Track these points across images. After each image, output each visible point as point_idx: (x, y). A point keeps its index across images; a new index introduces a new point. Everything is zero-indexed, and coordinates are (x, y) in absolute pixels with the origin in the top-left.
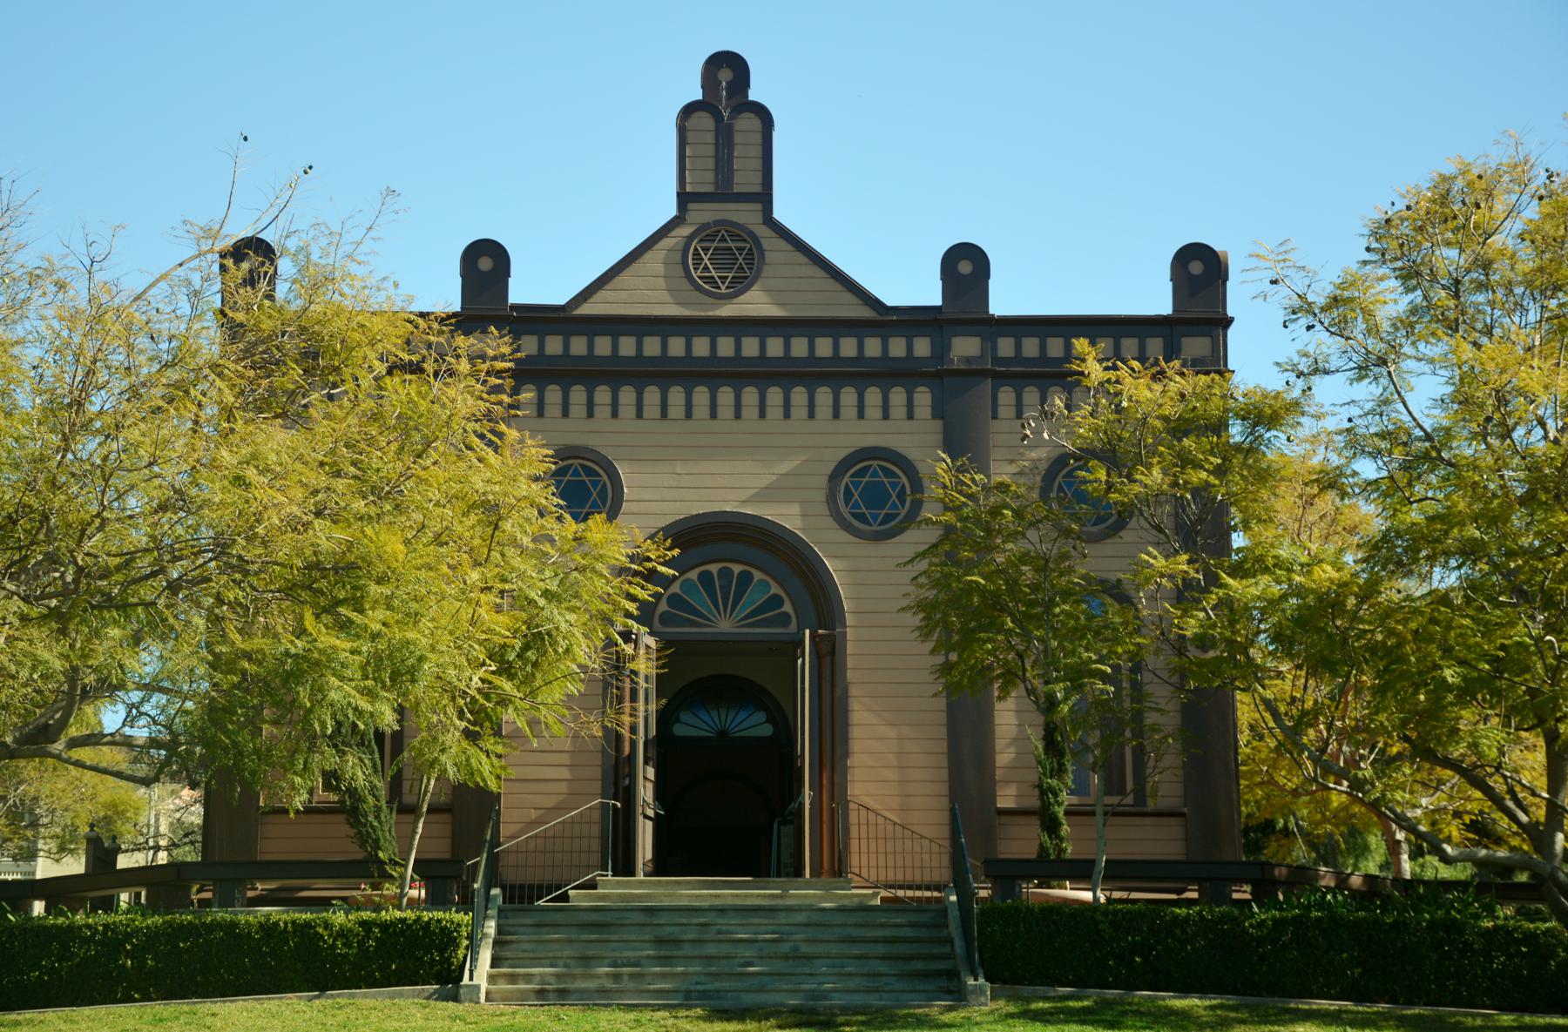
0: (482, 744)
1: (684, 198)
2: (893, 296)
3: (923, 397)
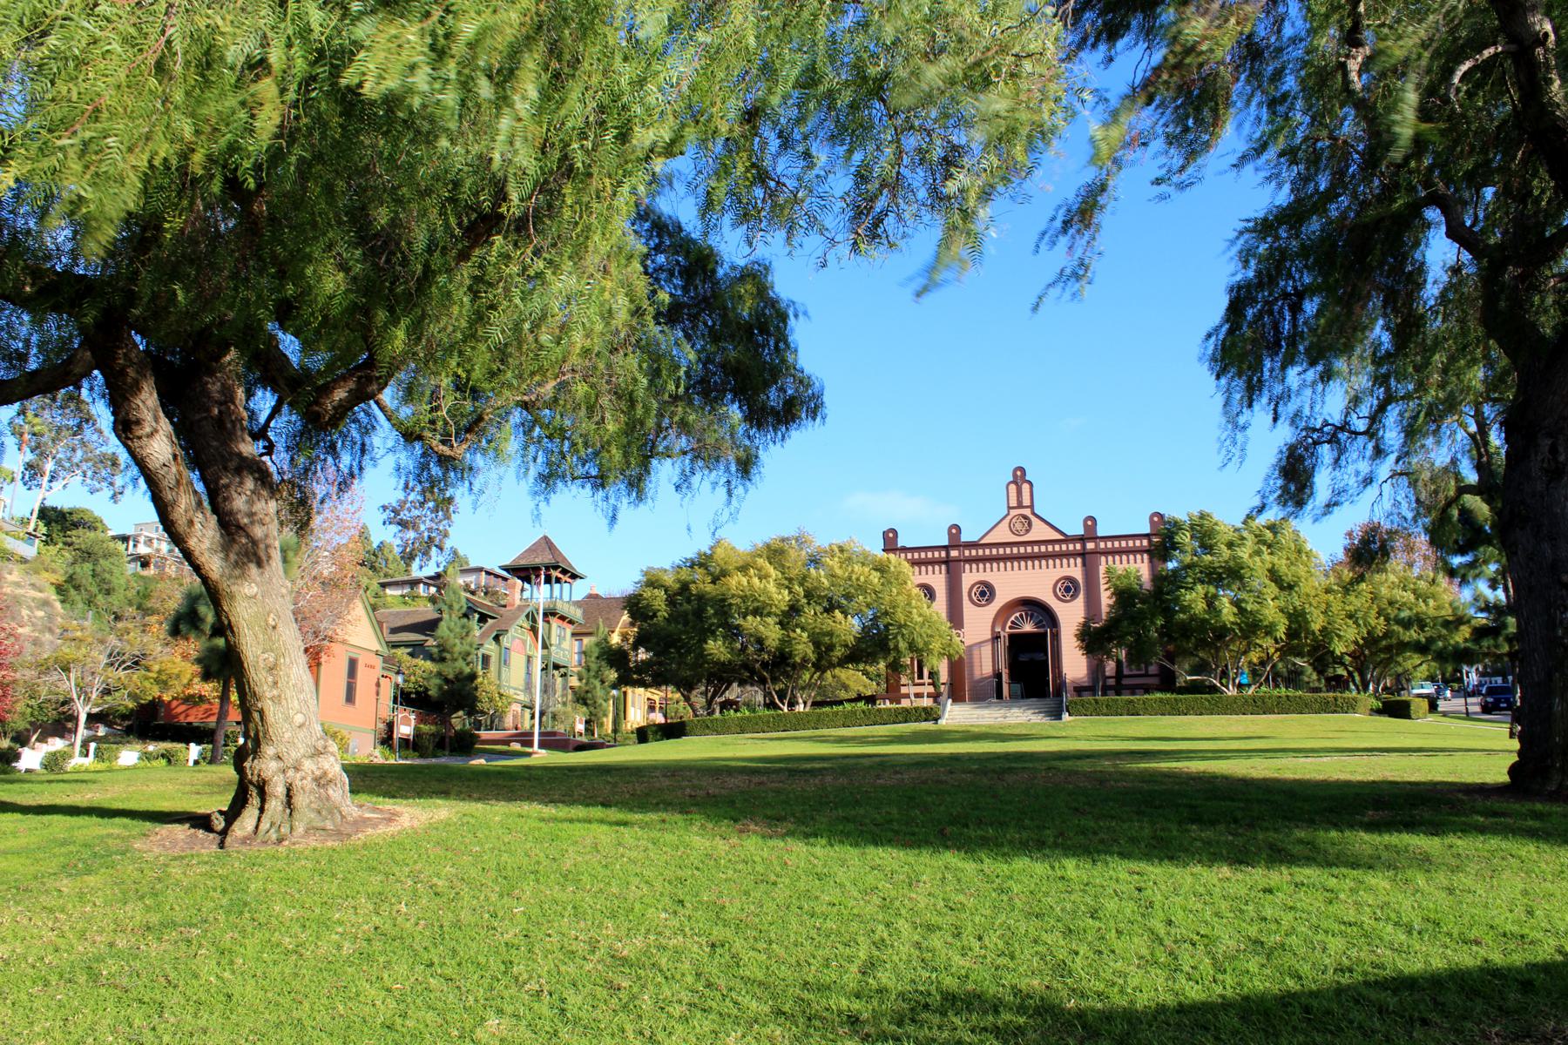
1: (1010, 508)
3: (1079, 560)
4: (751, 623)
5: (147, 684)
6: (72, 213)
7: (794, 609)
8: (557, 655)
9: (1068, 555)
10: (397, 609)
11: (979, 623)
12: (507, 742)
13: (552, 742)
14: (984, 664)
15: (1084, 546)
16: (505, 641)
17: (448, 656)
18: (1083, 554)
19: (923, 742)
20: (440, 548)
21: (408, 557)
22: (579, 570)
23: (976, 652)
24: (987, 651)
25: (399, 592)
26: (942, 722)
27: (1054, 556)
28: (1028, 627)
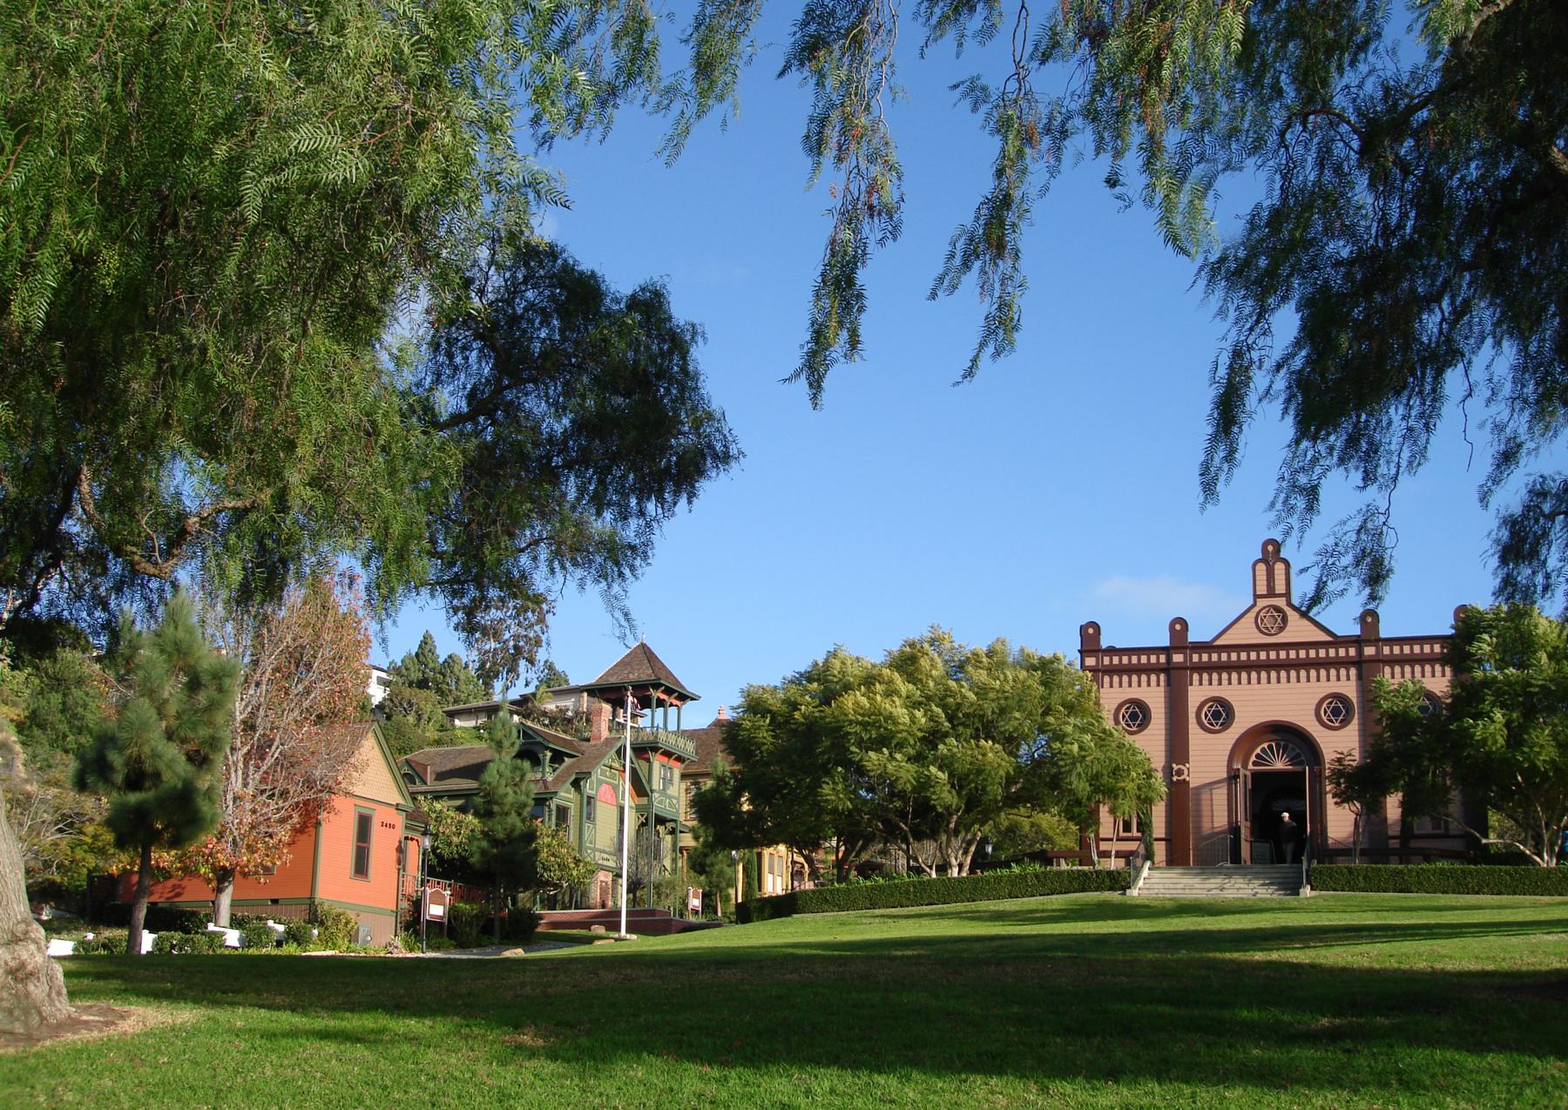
0: (225, 560)
1: (1256, 596)
2: (1341, 631)
3: (1353, 671)
4: (874, 759)
5: (79, 854)
6: (386, 172)
7: (933, 737)
8: (660, 805)
9: (1337, 663)
10: (467, 746)
11: (1209, 756)
12: (586, 925)
13: (644, 922)
14: (1217, 813)
15: (1360, 652)
16: (588, 788)
17: (496, 808)
18: (1359, 663)
19: (1075, 919)
20: (531, 661)
21: (487, 675)
22: (690, 687)
23: (1205, 796)
24: (1220, 796)
25: (472, 723)
26: (1134, 892)
27: (1317, 664)
28: (1280, 765)
